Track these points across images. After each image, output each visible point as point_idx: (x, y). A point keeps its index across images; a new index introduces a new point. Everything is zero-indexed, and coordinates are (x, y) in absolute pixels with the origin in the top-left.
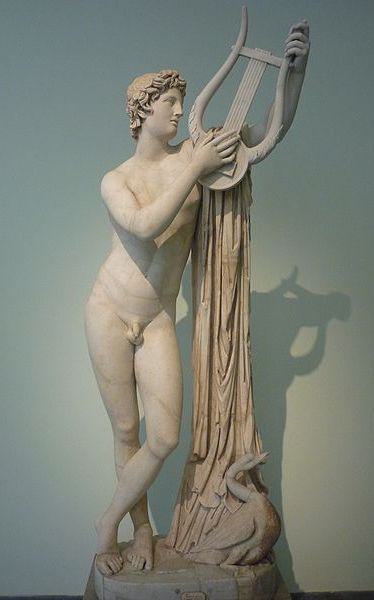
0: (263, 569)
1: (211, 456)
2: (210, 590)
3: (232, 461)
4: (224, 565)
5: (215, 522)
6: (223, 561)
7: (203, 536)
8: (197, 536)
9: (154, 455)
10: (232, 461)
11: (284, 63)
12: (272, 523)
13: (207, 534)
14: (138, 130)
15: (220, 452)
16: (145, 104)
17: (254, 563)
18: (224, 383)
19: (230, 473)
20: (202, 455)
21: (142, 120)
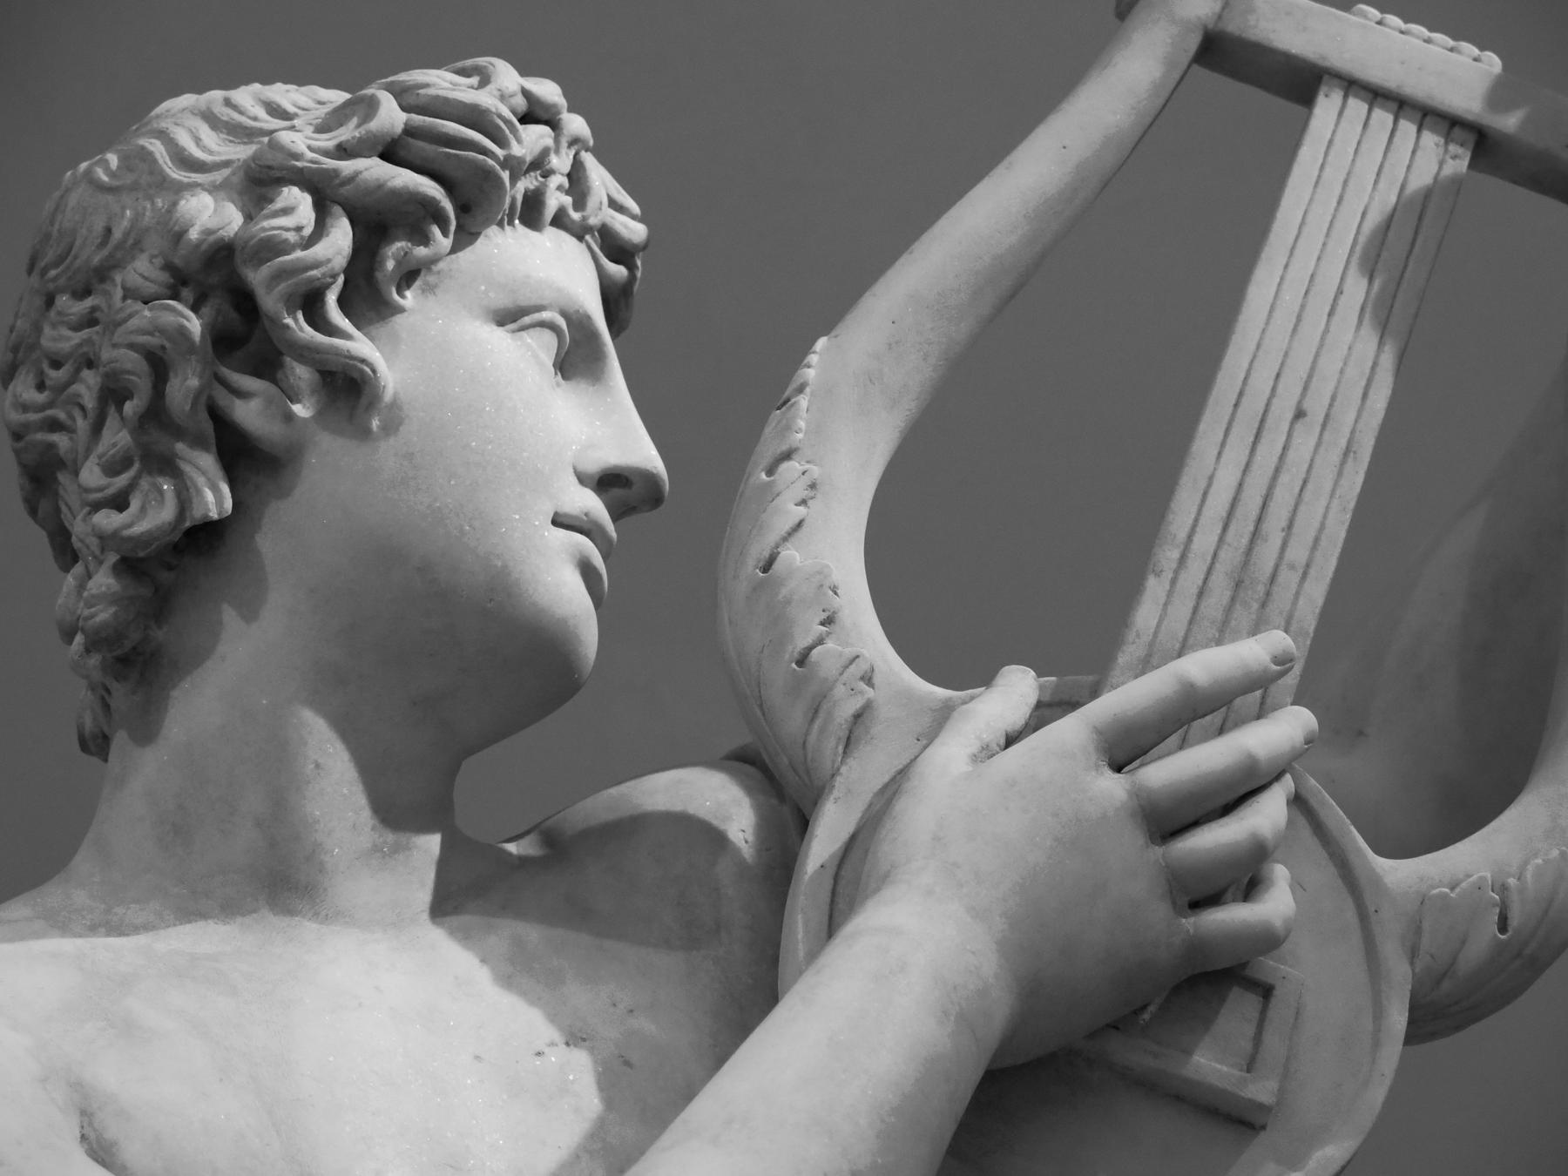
16: (311, 304)
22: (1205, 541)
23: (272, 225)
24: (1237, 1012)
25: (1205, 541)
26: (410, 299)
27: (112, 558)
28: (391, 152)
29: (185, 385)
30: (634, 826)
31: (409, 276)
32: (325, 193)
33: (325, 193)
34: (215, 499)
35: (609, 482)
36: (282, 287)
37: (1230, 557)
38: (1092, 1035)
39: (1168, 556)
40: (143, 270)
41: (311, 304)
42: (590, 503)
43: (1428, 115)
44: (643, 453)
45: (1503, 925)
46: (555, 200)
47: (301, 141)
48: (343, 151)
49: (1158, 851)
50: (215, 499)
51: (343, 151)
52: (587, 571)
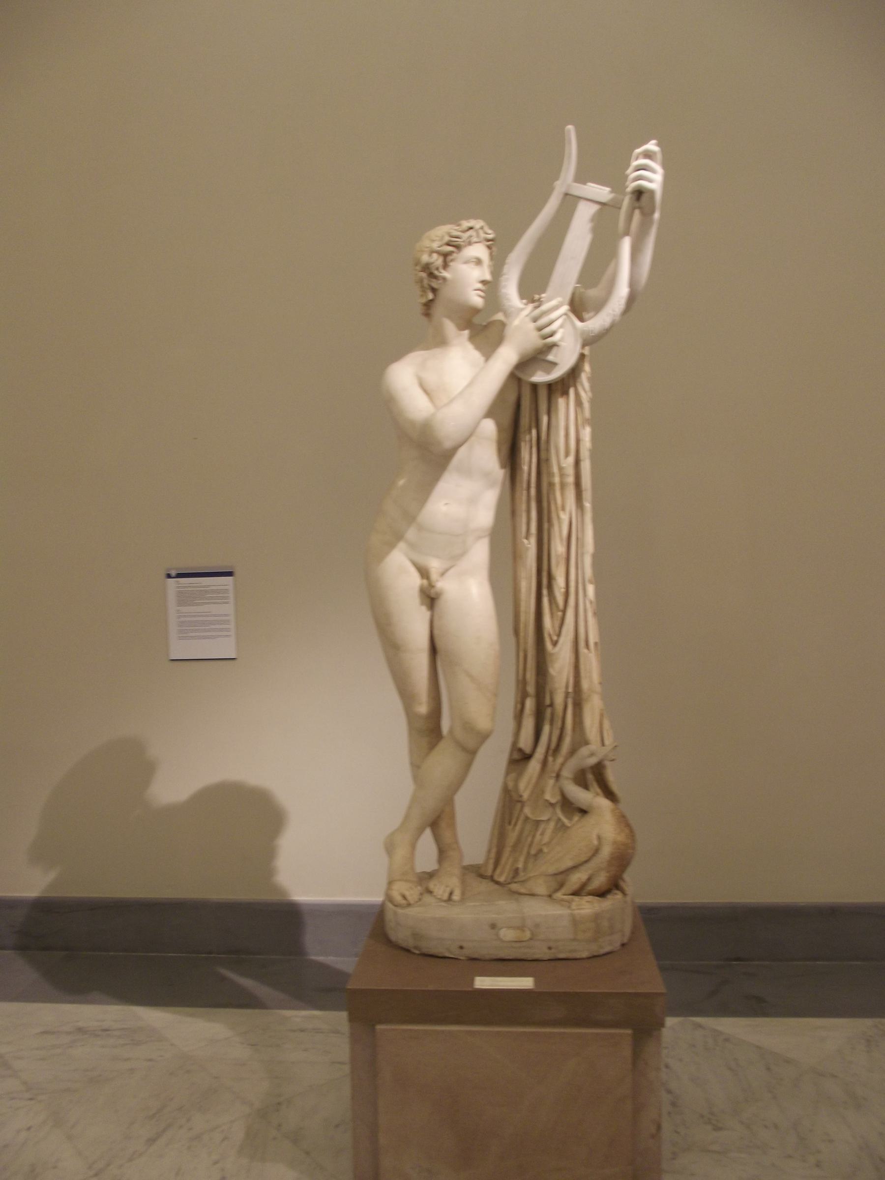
2: (537, 926)
4: (559, 895)
15: (553, 745)
21: (434, 290)
23: (432, 260)
24: (555, 350)
26: (451, 264)
28: (448, 244)
29: (426, 282)
30: (495, 321)
31: (452, 260)
32: (438, 253)
33: (438, 253)
34: (431, 296)
35: (484, 282)
41: (437, 269)
42: (480, 286)
44: (488, 277)
46: (475, 239)
47: (435, 245)
48: (441, 246)
49: (540, 332)
50: (431, 296)
51: (441, 246)
52: (480, 296)
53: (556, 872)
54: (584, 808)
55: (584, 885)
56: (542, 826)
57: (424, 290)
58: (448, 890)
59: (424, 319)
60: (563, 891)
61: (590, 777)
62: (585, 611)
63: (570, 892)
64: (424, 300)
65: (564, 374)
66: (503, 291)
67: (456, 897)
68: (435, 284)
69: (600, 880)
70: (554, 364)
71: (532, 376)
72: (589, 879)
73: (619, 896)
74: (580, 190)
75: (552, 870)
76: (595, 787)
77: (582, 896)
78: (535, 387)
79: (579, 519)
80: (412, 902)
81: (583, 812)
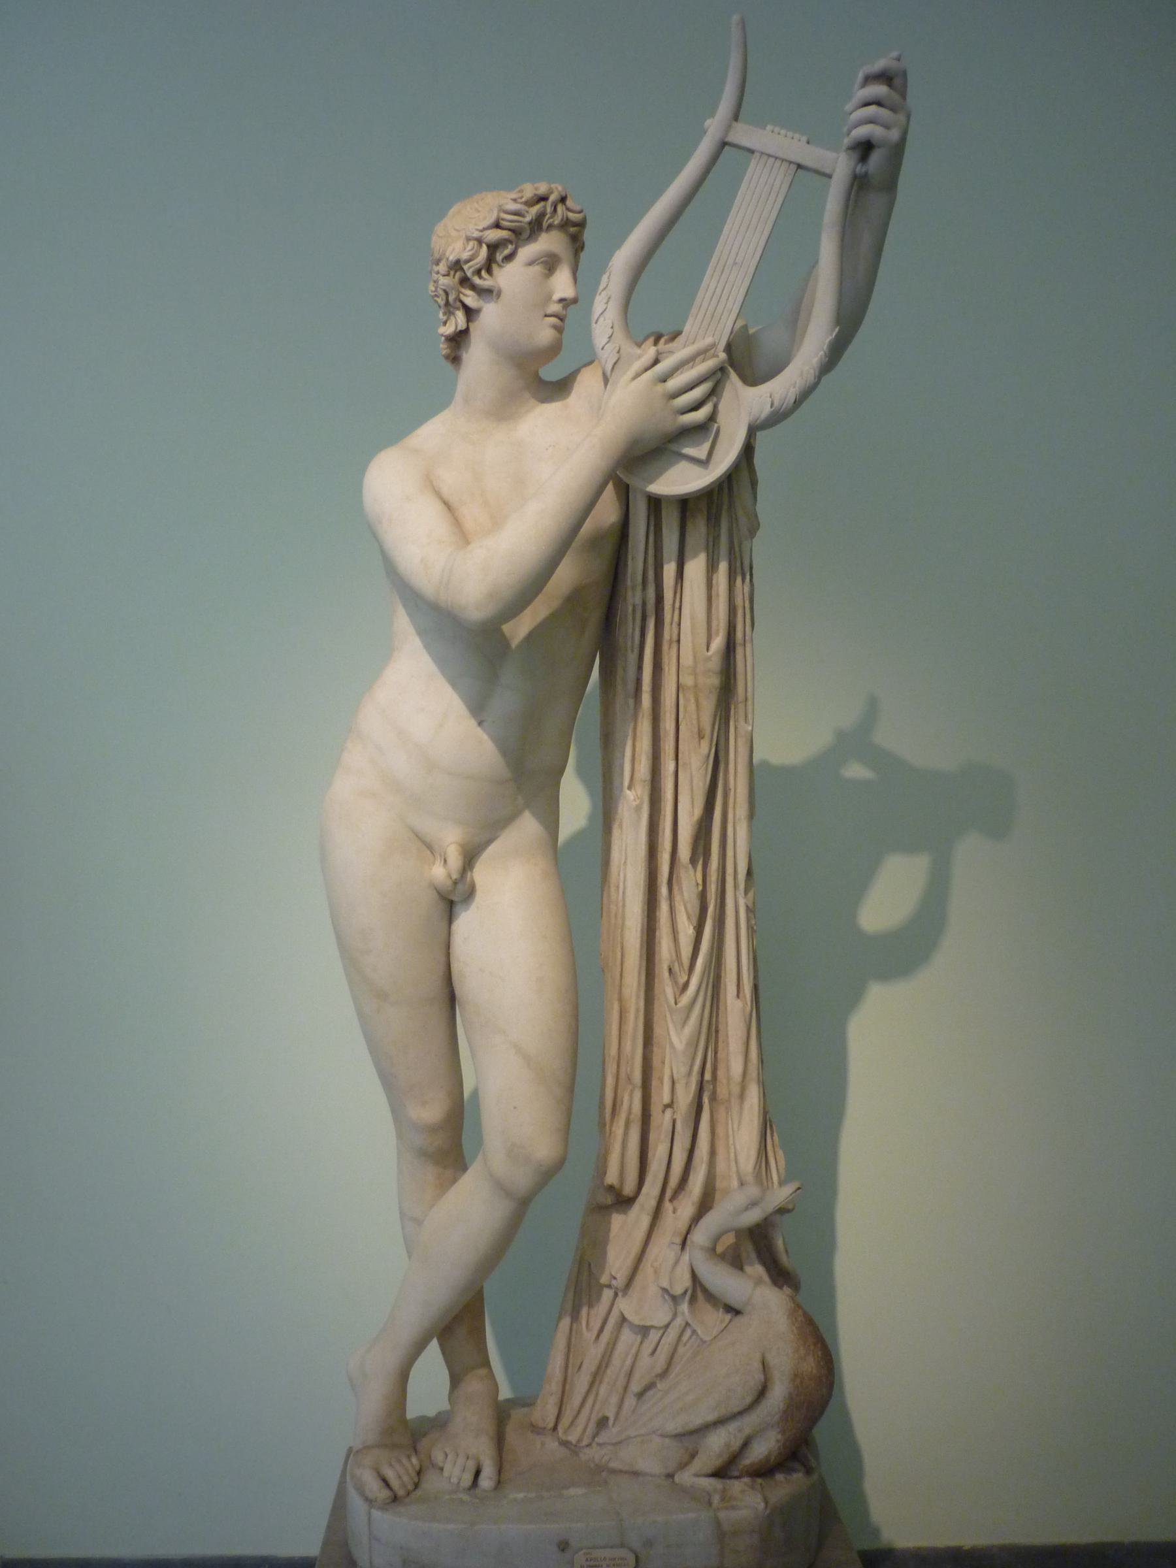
0: (785, 1486)
1: (651, 1190)
2: (649, 1543)
3: (705, 1205)
5: (659, 1370)
6: (683, 1466)
7: (630, 1401)
8: (614, 1400)
9: (500, 1187)
10: (705, 1205)
11: (841, 165)
12: (810, 1366)
13: (640, 1395)
14: (459, 340)
17: (764, 1472)
18: (685, 999)
19: (700, 1236)
20: (629, 1189)
21: (470, 313)
22: (705, 304)
25: (705, 304)
27: (443, 338)
36: (471, 270)
37: (711, 309)
38: (664, 444)
39: (694, 310)
40: (442, 268)
43: (775, 162)
45: (772, 406)
53: (680, 1430)
54: (737, 1306)
55: (734, 1458)
56: (654, 1336)
57: (449, 308)
58: (471, 1466)
59: (448, 365)
60: (697, 1465)
61: (748, 1250)
62: (634, 619)
63: (709, 1471)
64: (449, 329)
65: (712, 483)
66: (702, 419)
67: (486, 1482)
68: (470, 299)
69: (764, 1448)
70: (531, 263)
71: (651, 482)
72: (746, 1444)
73: (798, 1476)
74: (743, 135)
75: (673, 1426)
76: (757, 1269)
77: (731, 1478)
78: (655, 503)
79: (722, 732)
80: (401, 1493)
81: (734, 1311)
